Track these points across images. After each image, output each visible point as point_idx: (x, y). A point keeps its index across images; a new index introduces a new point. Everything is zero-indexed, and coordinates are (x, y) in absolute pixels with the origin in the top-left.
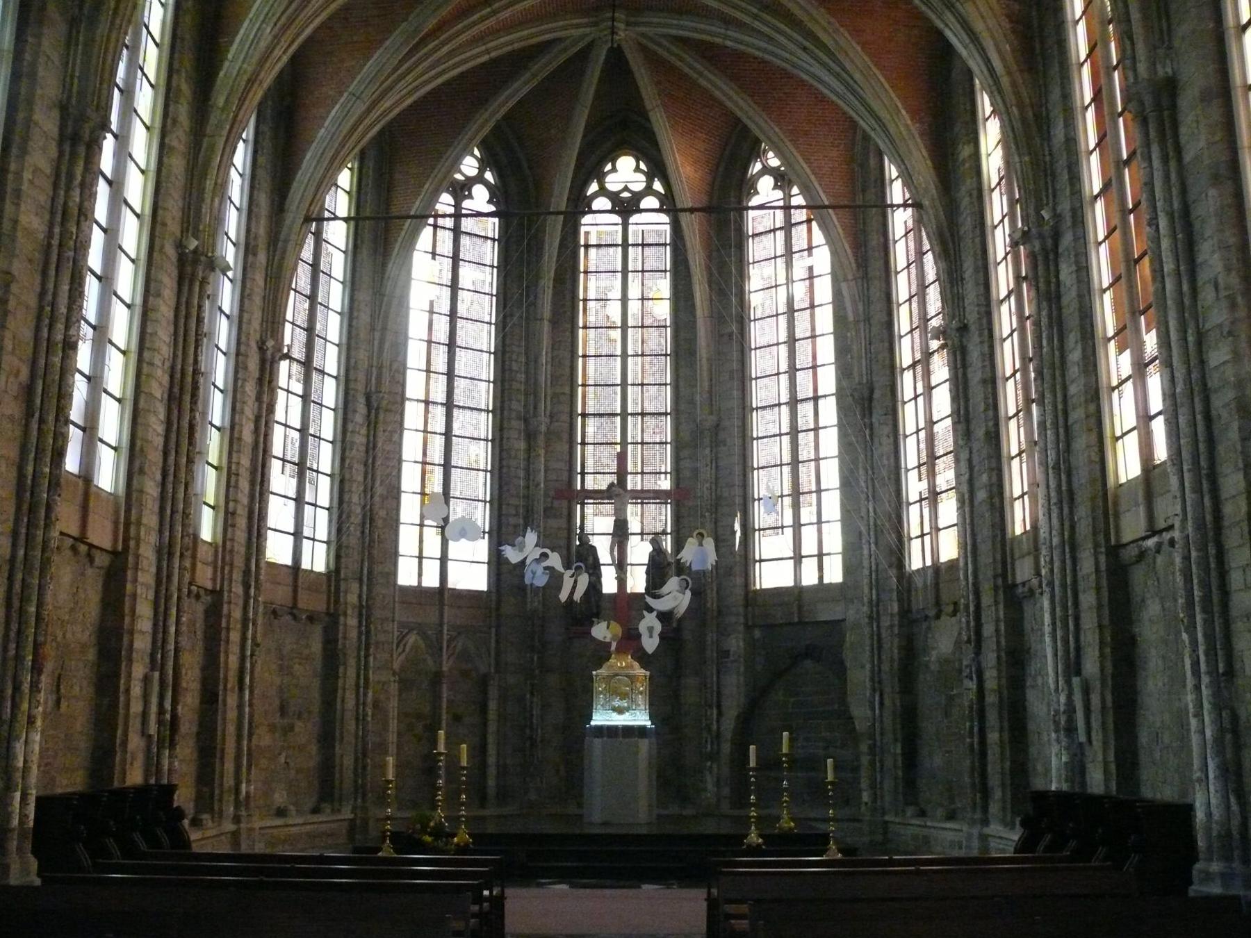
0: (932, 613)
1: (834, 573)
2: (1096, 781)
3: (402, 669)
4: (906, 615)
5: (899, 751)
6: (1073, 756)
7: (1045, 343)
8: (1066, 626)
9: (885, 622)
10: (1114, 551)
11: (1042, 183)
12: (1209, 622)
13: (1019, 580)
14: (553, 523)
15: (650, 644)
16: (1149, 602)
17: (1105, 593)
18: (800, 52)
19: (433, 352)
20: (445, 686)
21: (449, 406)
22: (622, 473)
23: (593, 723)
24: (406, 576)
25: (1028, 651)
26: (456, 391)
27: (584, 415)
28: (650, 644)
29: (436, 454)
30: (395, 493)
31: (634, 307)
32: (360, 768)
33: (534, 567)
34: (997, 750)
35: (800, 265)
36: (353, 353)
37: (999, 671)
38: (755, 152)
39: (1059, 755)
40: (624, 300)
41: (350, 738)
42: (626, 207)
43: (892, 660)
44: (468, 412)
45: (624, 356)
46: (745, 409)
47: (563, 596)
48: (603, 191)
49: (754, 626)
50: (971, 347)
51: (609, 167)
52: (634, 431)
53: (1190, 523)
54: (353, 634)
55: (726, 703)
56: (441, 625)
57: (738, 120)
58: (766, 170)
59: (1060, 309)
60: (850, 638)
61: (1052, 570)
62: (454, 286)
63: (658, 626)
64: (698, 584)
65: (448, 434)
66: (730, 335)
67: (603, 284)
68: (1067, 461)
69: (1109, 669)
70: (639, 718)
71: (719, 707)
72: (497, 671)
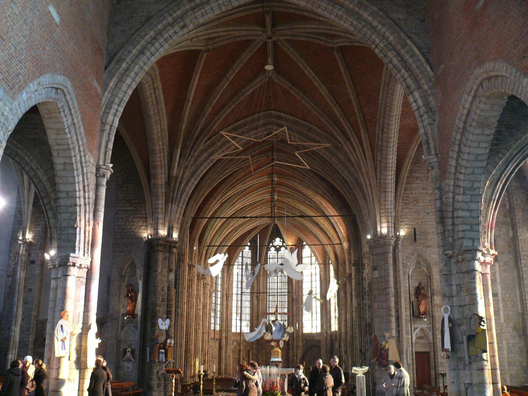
4: (331, 340)
9: (328, 341)
15: (281, 346)
22: (277, 307)
24: (234, 330)
29: (239, 305)
30: (231, 313)
32: (226, 369)
41: (224, 363)
42: (278, 249)
45: (277, 283)
54: (224, 342)
55: (298, 356)
60: (322, 343)
64: (291, 335)
65: (241, 300)
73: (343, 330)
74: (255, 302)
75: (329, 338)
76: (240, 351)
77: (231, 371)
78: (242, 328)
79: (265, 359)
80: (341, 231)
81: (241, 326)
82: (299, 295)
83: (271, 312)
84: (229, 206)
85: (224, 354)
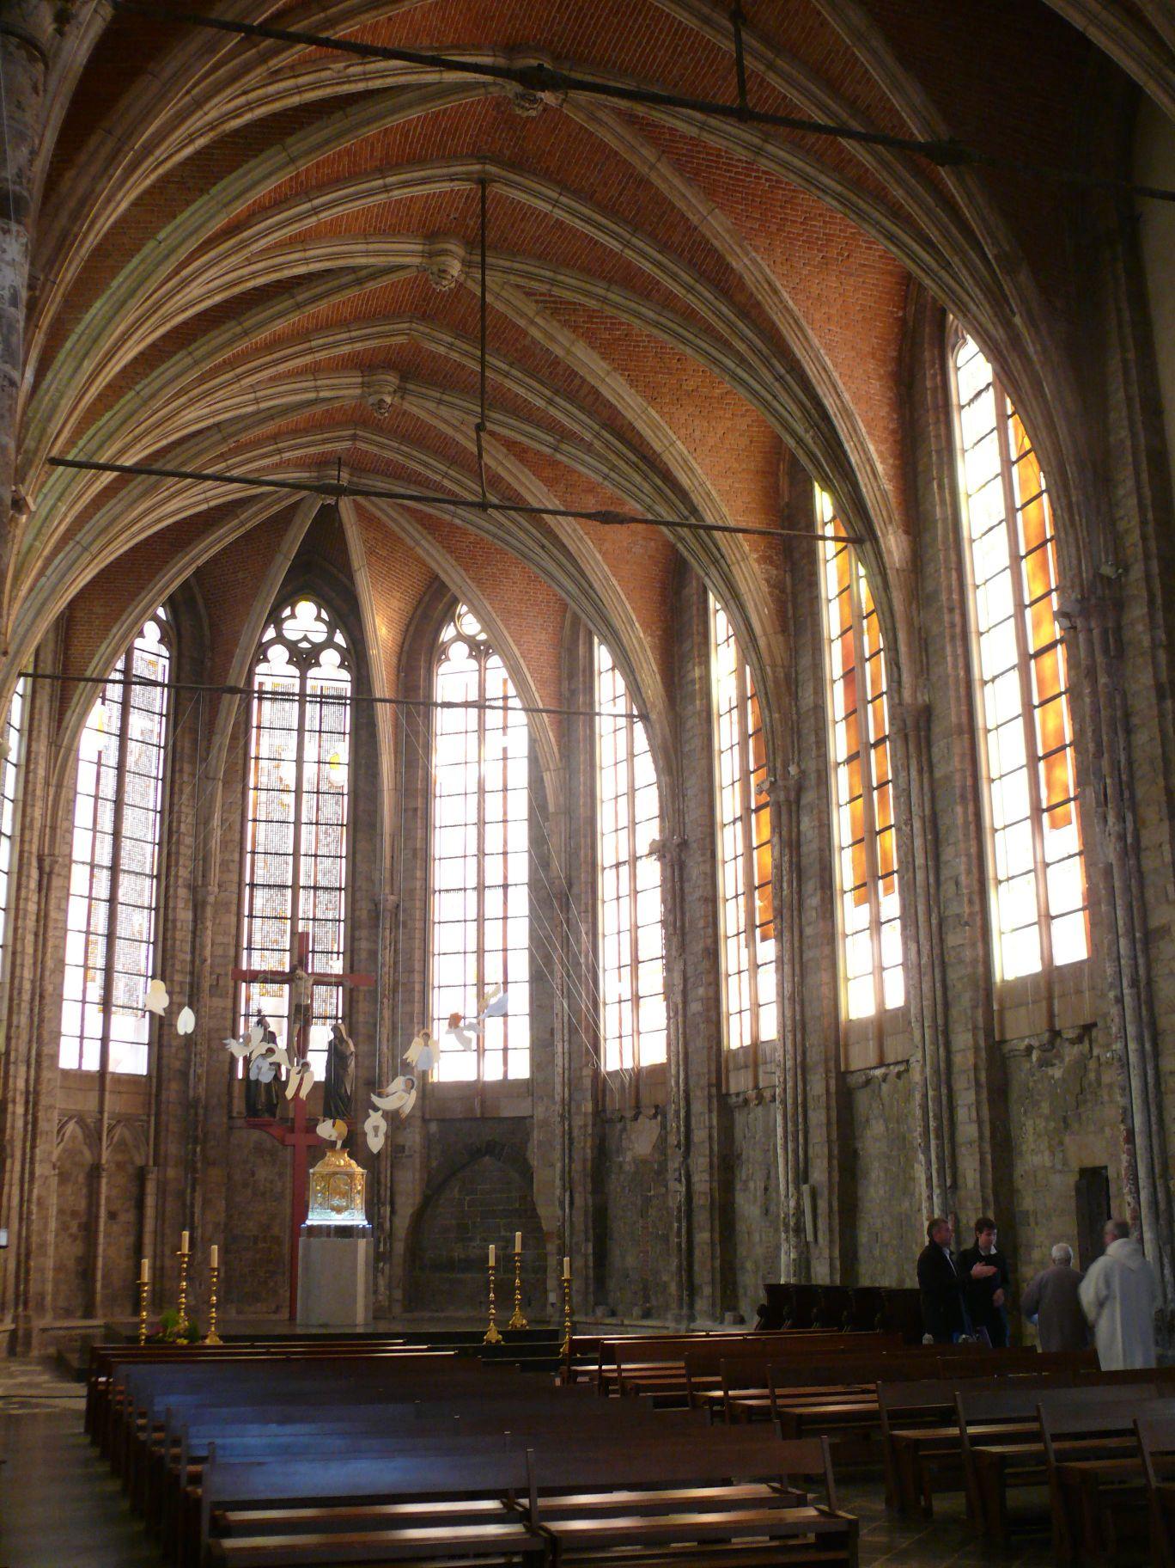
0: (629, 1114)
1: (520, 1069)
2: (822, 1274)
3: (59, 1159)
4: (601, 1117)
5: (590, 1251)
6: (800, 1254)
7: (785, 885)
8: (796, 1139)
9: (578, 1121)
10: (842, 1076)
11: (789, 740)
12: (940, 1147)
13: (733, 1090)
14: (218, 1002)
15: (376, 1143)
16: (873, 1122)
17: (834, 1114)
18: (538, 550)
19: (100, 809)
20: (104, 1181)
21: (115, 869)
23: (308, 1223)
24: (67, 1059)
25: (739, 1156)
26: (123, 854)
27: (253, 886)
28: (376, 1143)
29: (100, 924)
30: (61, 964)
31: (310, 771)
33: (260, 1062)
34: (707, 1249)
35: (494, 741)
36: (29, 810)
37: (711, 1175)
38: (449, 615)
39: (788, 1253)
40: (299, 762)
42: (305, 658)
43: (585, 1160)
44: (133, 877)
45: (298, 823)
46: (427, 891)
47: (290, 1093)
48: (280, 639)
49: (430, 1120)
50: (690, 863)
51: (287, 612)
52: (305, 907)
53: (928, 1069)
54: (20, 1123)
55: (400, 1200)
56: (101, 1112)
57: (437, 577)
58: (460, 637)
59: (799, 855)
60: (537, 1135)
61: (785, 1090)
62: (123, 736)
63: (383, 1126)
65: (112, 900)
66: (416, 810)
67: (277, 742)
68: (801, 993)
69: (836, 1177)
70: (356, 1218)
71: (392, 1204)
72: (155, 1164)
73: (673, 1059)
74: (184, 915)
75: (588, 1107)
76: (95, 1172)
77: (49, 1287)
78: (112, 1047)
79: (222, 1218)
80: (869, 460)
81: (105, 1040)
82: (412, 891)
83: (256, 966)
84: (193, 244)
85: (16, 1191)
